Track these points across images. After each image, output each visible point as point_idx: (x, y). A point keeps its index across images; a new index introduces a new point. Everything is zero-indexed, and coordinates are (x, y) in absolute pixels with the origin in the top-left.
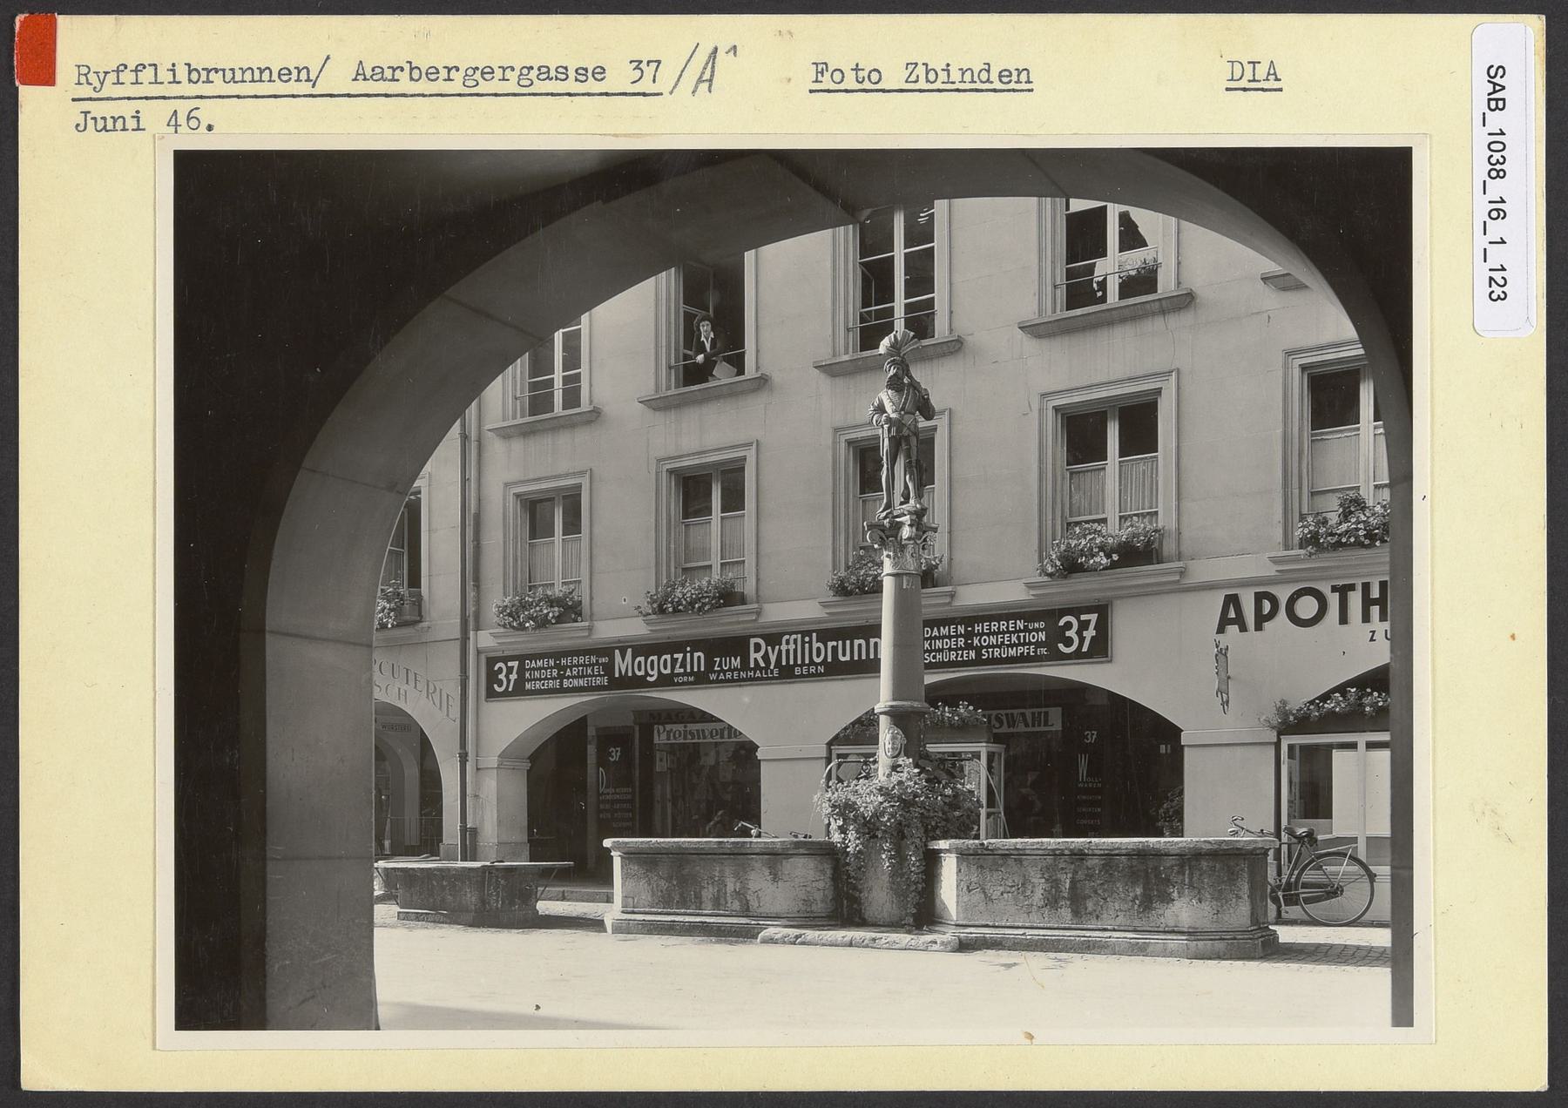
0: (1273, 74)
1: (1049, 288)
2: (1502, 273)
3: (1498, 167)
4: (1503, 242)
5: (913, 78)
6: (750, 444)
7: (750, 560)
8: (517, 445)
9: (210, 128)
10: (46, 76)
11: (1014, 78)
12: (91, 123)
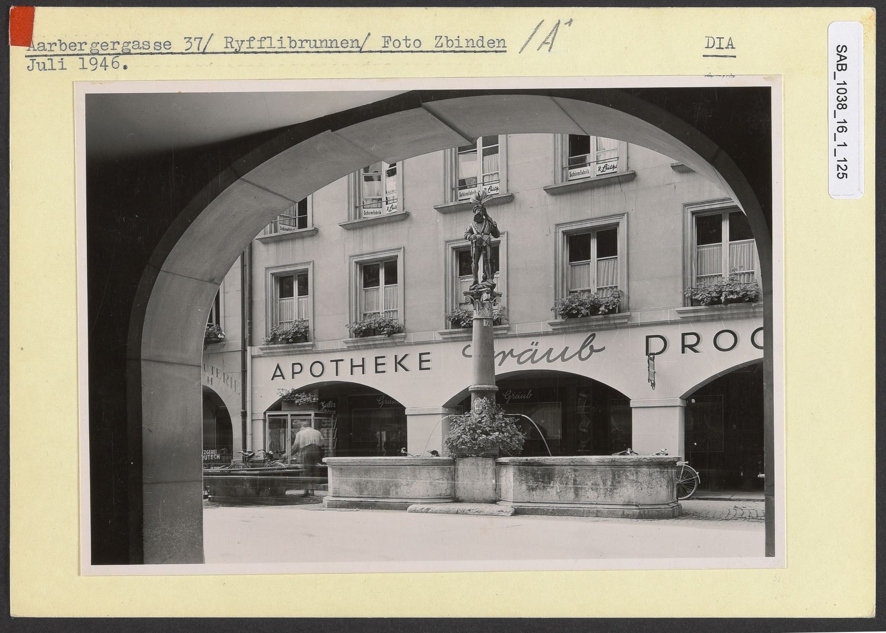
0: (731, 46)
1: (560, 169)
2: (845, 163)
3: (843, 103)
4: (845, 145)
5: (439, 45)
6: (400, 249)
7: (401, 310)
8: (272, 248)
9: (125, 67)
10: (26, 40)
11: (350, 45)
12: (36, 65)
